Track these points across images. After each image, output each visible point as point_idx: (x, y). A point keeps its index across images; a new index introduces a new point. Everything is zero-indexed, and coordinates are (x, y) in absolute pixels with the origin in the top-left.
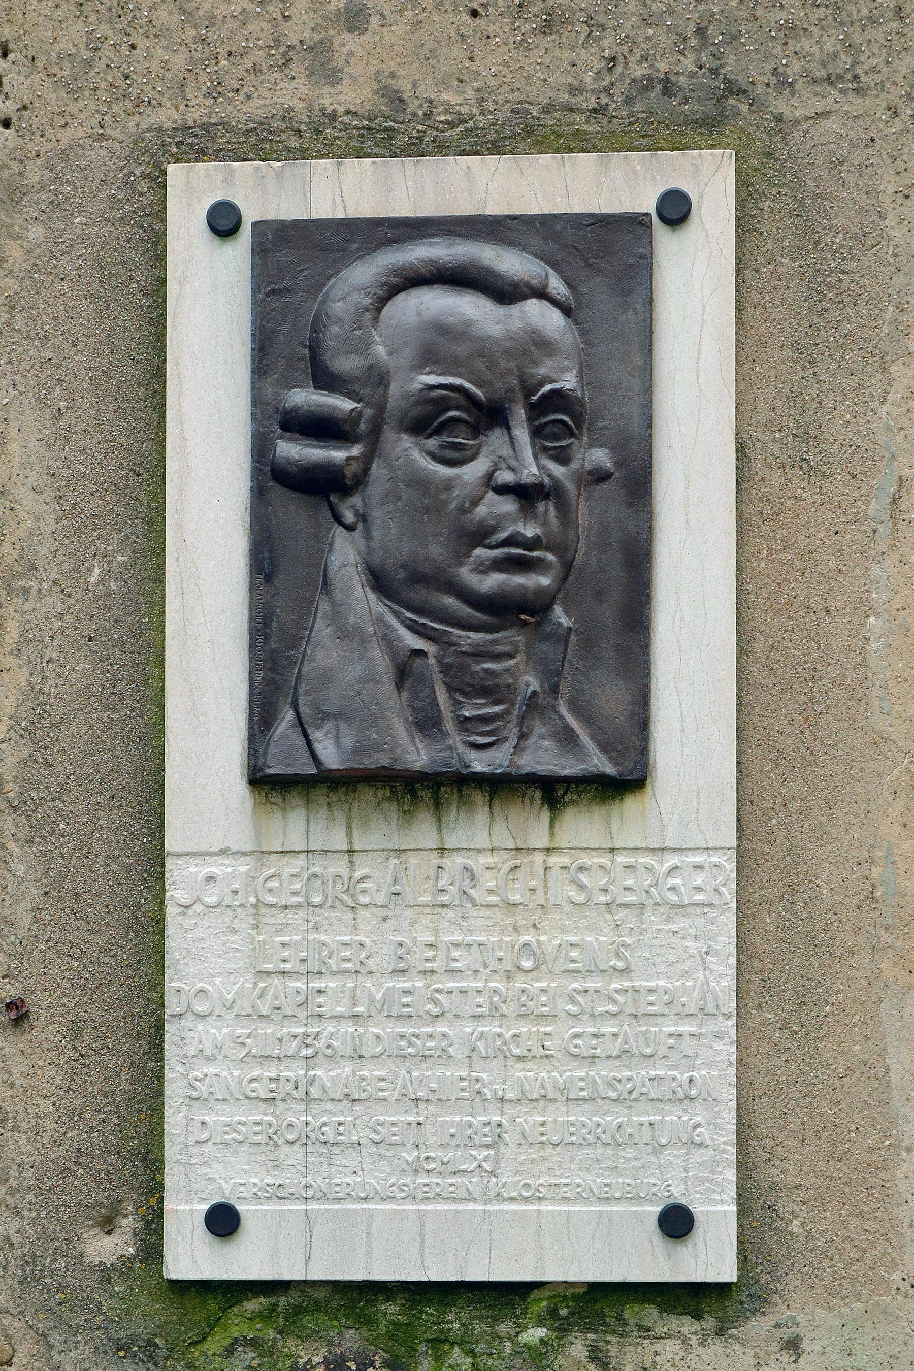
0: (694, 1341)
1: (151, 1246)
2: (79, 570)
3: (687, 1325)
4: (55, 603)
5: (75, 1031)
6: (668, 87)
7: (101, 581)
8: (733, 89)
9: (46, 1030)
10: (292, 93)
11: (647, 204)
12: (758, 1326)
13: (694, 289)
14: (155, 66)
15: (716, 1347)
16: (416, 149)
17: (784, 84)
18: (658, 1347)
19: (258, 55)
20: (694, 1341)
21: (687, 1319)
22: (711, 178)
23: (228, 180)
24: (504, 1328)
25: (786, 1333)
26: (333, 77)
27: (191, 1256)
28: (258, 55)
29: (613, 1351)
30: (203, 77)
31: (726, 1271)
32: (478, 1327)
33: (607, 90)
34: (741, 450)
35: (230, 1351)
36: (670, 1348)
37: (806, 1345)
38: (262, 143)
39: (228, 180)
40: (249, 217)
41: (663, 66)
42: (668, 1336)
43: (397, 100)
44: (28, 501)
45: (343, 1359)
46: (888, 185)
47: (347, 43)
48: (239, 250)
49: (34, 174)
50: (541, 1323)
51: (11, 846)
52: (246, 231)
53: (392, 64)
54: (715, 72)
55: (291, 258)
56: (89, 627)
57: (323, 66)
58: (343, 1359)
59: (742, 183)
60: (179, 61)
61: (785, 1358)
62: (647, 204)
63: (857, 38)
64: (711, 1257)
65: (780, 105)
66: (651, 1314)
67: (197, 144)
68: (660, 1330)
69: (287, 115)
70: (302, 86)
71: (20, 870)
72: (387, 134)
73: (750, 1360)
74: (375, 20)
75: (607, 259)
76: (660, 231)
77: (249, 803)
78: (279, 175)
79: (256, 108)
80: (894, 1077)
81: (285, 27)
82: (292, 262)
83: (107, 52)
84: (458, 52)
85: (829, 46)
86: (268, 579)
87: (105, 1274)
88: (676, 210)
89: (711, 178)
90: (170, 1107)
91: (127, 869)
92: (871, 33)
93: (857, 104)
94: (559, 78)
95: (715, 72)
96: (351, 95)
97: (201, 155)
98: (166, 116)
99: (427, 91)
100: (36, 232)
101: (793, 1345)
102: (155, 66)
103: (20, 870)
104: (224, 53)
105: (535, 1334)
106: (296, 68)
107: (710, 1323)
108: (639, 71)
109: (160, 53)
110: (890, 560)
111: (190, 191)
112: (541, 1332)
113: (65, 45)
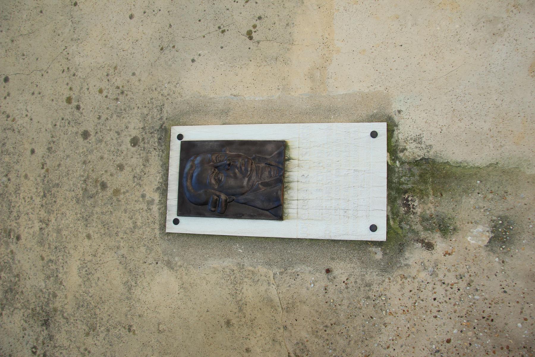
0: (399, 131)
1: (379, 244)
2: (239, 254)
3: (396, 133)
4: (245, 260)
5: (333, 259)
6: (160, 139)
7: (242, 249)
8: (161, 127)
9: (331, 265)
10: (155, 208)
11: (180, 142)
12: (396, 119)
13: (195, 133)
14: (149, 234)
15: (400, 127)
16: (167, 185)
17: (161, 118)
18: (400, 139)
19: (148, 214)
20: (399, 131)
21: (395, 133)
22: (176, 130)
23: (169, 221)
24: (397, 170)
25: (397, 113)
26: (153, 200)
27: (381, 235)
28: (148, 214)
29: (401, 147)
30: (151, 225)
31: (385, 125)
32: (396, 175)
33: (159, 150)
34: (224, 124)
35: (401, 228)
36: (400, 136)
37: (399, 109)
38: (164, 215)
39: (169, 221)
40: (176, 217)
41: (156, 140)
42: (398, 136)
43: (158, 188)
44: (226, 264)
45: (403, 204)
46: (179, 99)
47: (148, 198)
48: (181, 219)
49: (166, 258)
50: (395, 162)
51: (294, 271)
52: (179, 218)
53: (152, 189)
54: (158, 131)
55: (184, 209)
56: (251, 252)
57: (151, 202)
58: (403, 204)
59: (177, 125)
60: (148, 229)
61: (402, 113)
62: (180, 142)
63: (155, 106)
64: (381, 128)
65: (164, 119)
66: (393, 140)
67: (163, 226)
68: (396, 138)
69: (159, 209)
70: (154, 206)
71: (299, 269)
72: (163, 190)
73: (402, 120)
74: (144, 192)
75: (189, 149)
76: (184, 140)
77: (287, 220)
78: (169, 211)
79: (157, 215)
80: (345, 93)
81: (144, 209)
82: (184, 209)
83: (146, 243)
84: (150, 177)
85: (156, 111)
86: (243, 215)
87: (385, 254)
88: (180, 137)
89: (176, 130)
90: (483, 241)
91: (299, 247)
92: (154, 104)
93: (166, 106)
94: (157, 158)
95: (158, 131)
96: (156, 197)
97: (165, 226)
98: (157, 232)
99: (156, 183)
100: (177, 259)
101: (399, 112)
102: (149, 234)
103: (299, 269)
104: (147, 221)
105: (398, 163)
106: (151, 208)
107: (395, 128)
108: (157, 144)
109: (147, 233)
110: (246, 96)
111: (171, 228)
112: (397, 162)
113: (144, 251)
